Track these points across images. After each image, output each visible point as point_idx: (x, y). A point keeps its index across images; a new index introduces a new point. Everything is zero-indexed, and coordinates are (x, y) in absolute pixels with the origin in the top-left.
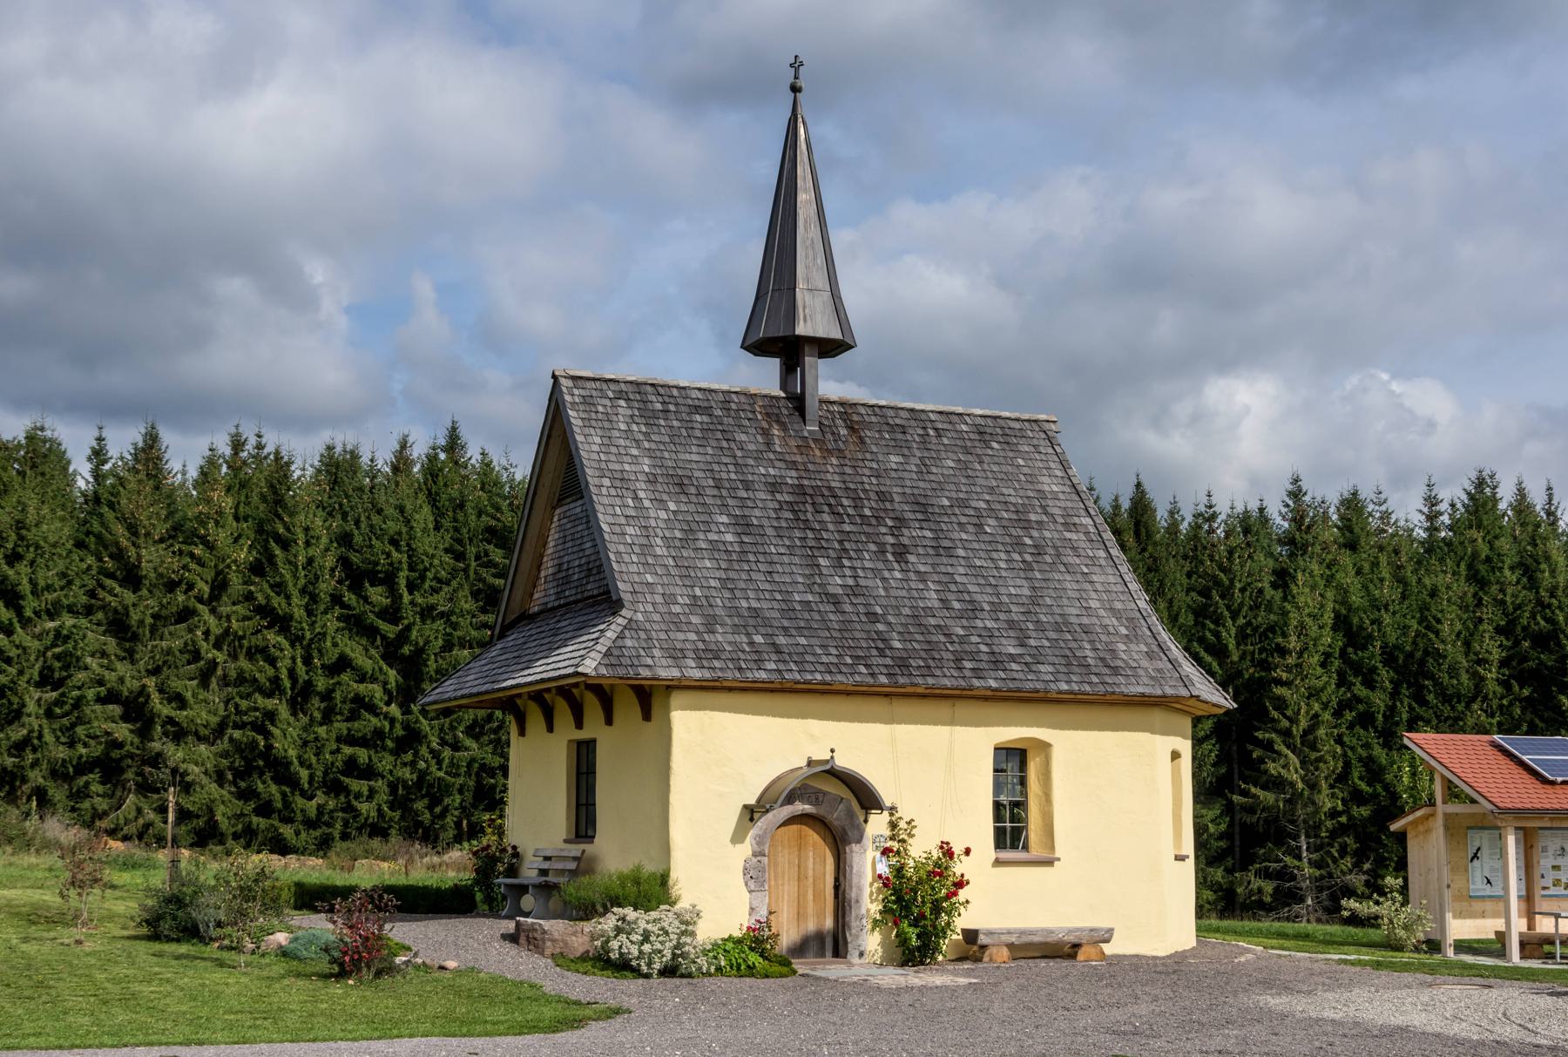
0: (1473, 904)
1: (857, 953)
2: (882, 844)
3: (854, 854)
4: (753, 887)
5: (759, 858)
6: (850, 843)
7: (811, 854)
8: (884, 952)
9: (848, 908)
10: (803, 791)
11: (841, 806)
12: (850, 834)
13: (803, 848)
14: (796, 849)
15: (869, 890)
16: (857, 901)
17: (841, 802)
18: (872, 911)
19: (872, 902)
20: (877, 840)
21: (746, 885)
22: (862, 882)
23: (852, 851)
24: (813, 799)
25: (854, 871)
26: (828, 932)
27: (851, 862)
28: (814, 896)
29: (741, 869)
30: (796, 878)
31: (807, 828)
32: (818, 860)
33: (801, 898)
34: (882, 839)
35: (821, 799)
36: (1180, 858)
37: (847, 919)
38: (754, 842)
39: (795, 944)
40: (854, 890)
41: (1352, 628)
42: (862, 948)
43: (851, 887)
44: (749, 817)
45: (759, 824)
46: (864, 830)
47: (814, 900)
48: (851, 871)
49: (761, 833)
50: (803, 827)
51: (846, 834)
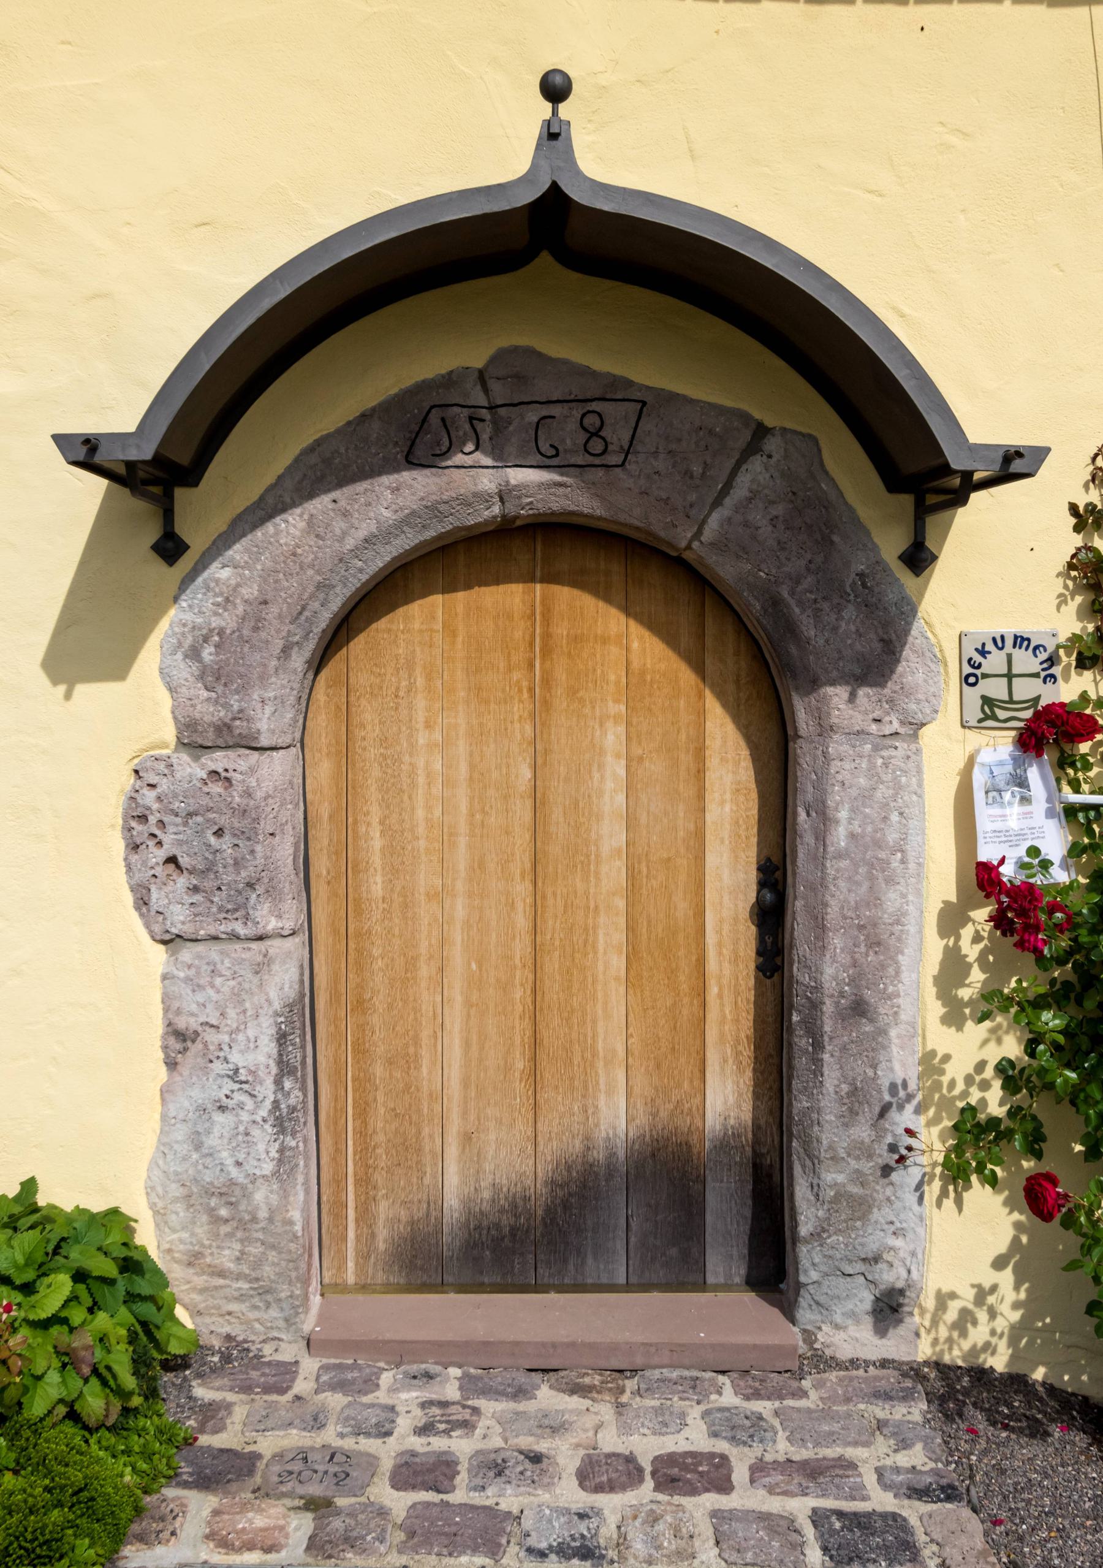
0: (528, 722)
1: (865, 1299)
2: (1024, 689)
3: (837, 746)
4: (179, 918)
5: (219, 760)
6: (814, 684)
7: (613, 737)
8: (1030, 1308)
9: (802, 1042)
10: (500, 392)
11: (754, 473)
12: (808, 628)
13: (560, 701)
14: (519, 708)
15: (934, 948)
16: (859, 1009)
17: (752, 448)
18: (957, 1070)
19: (954, 1018)
20: (995, 662)
21: (142, 902)
22: (892, 899)
23: (825, 729)
24: (570, 435)
25: (839, 837)
26: (724, 1145)
27: (820, 786)
28: (632, 957)
29: (113, 812)
30: (522, 859)
31: (587, 602)
32: (655, 767)
33: (552, 964)
34: (1025, 661)
35: (618, 434)
36: (113, 826)
37: (800, 1104)
38: (184, 671)
39: (516, 1205)
40: (837, 941)
41: (947, 1114)
42: (890, 1276)
43: (820, 927)
44: (152, 533)
45: (219, 572)
46: (907, 610)
47: (632, 980)
48: (821, 838)
49: (228, 621)
50: (564, 594)
51: (791, 629)
